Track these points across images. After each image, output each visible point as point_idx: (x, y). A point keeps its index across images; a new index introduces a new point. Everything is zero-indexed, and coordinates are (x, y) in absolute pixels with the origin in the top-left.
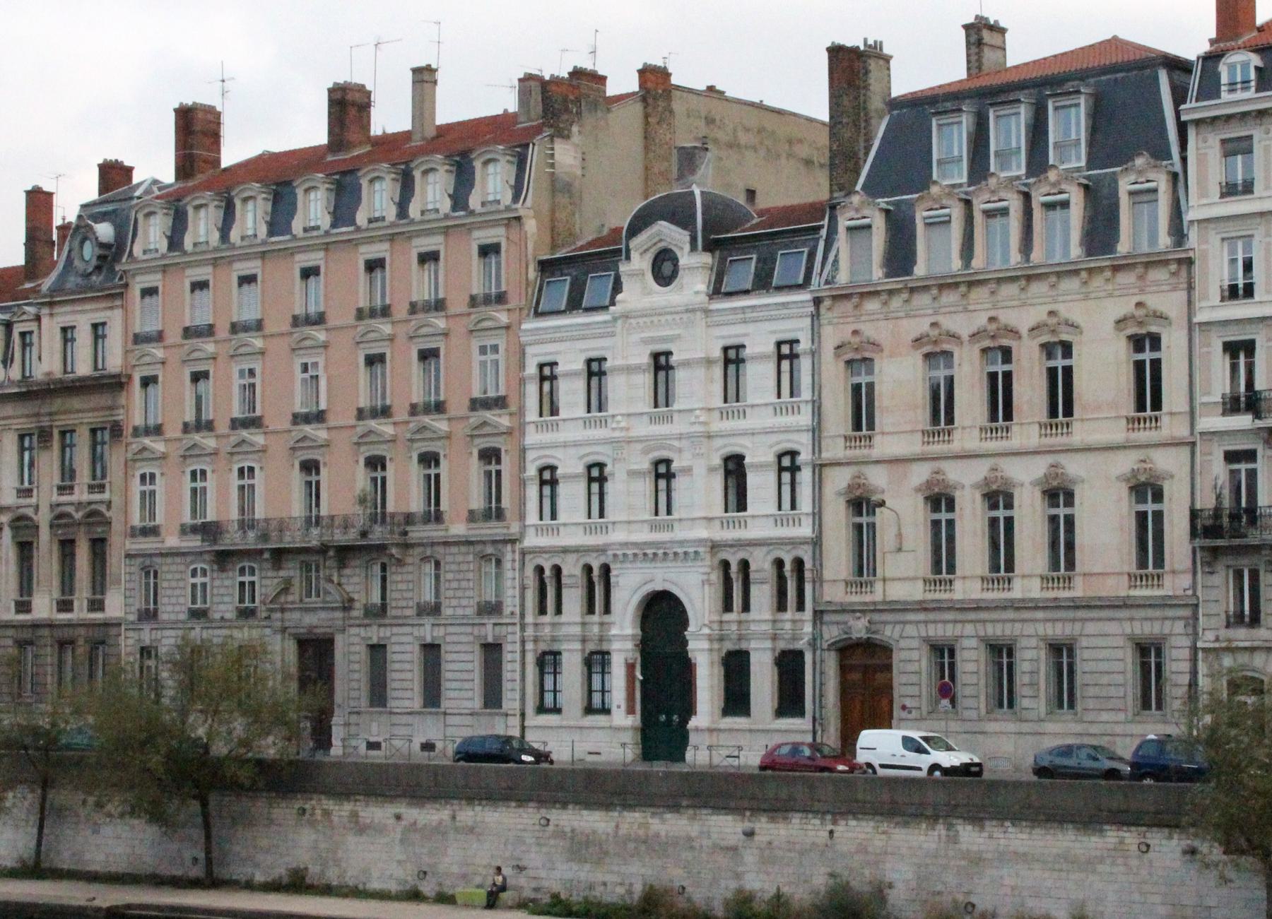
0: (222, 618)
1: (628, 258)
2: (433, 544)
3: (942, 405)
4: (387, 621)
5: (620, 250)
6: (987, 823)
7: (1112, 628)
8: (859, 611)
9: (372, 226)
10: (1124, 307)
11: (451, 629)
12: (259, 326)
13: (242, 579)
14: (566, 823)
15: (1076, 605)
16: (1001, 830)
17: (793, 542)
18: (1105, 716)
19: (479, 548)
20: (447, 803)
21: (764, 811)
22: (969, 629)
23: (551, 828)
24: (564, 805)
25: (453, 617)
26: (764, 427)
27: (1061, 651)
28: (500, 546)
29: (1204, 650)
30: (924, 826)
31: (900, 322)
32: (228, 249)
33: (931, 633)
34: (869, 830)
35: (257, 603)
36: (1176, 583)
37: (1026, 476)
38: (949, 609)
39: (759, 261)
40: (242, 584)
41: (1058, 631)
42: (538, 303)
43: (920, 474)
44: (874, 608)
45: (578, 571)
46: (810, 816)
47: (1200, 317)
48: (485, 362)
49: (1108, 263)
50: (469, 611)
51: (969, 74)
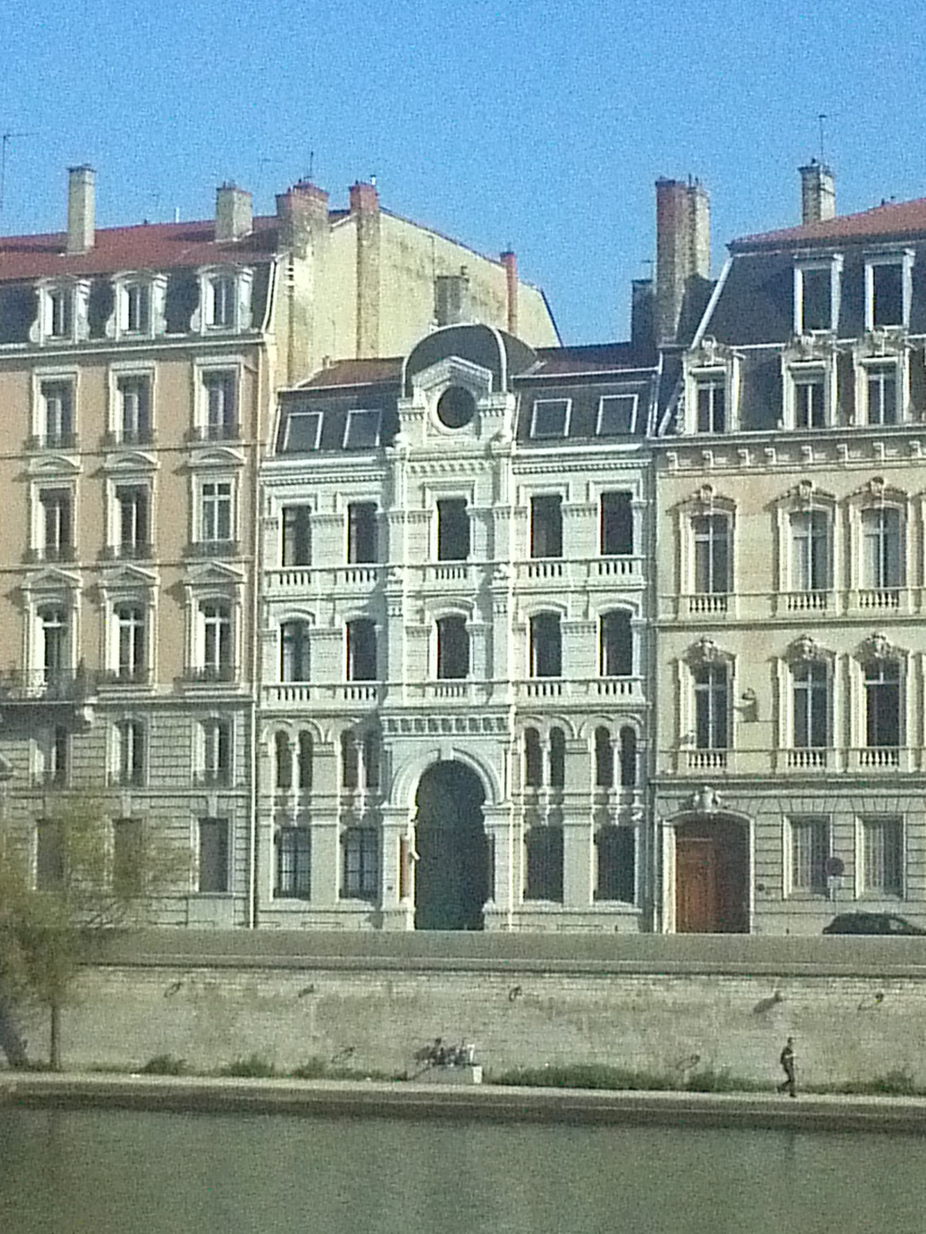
1: (410, 394)
17: (621, 710)
22: (844, 805)
26: (585, 584)
33: (870, 808)
42: (280, 441)
48: (211, 504)
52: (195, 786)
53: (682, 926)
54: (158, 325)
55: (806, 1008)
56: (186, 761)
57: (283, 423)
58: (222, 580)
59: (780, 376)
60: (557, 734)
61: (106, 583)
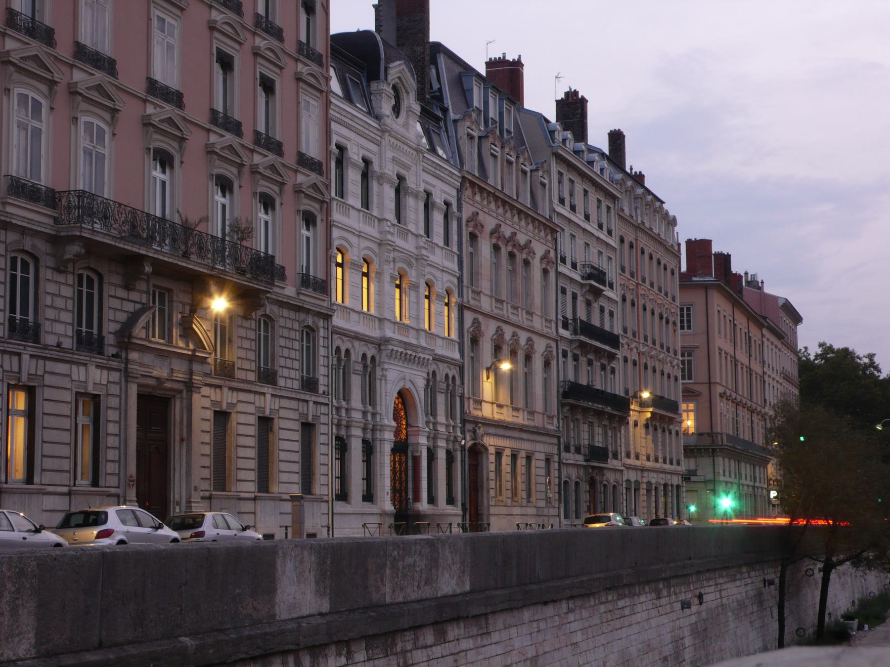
58: (109, 104)
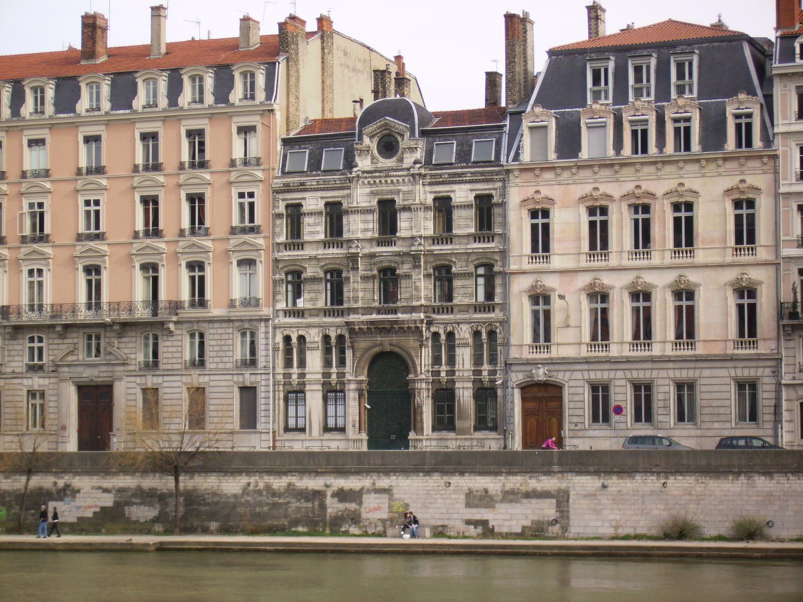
0: (13, 372)
2: (198, 322)
3: (599, 236)
4: (158, 373)
5: (354, 134)
6: (776, 475)
7: (723, 372)
8: (540, 364)
9: (145, 110)
10: (732, 181)
11: (213, 377)
12: (46, 173)
13: (32, 345)
14: (465, 485)
15: (698, 359)
16: (785, 478)
18: (716, 425)
19: (237, 324)
20: (367, 475)
21: (616, 472)
22: (620, 374)
23: (452, 488)
24: (462, 473)
25: (216, 369)
27: (685, 389)
28: (255, 323)
29: (786, 385)
30: (731, 478)
31: (569, 186)
32: (18, 121)
34: (692, 481)
35: (45, 360)
36: (764, 347)
37: (660, 283)
38: (606, 362)
39: (457, 145)
40: (31, 349)
41: (684, 375)
42: (284, 165)
43: (584, 280)
44: (551, 362)
45: (318, 339)
46: (648, 475)
47: (783, 190)
49: (721, 156)
50: (229, 366)
51: (590, 37)
52: (140, 369)
53: (525, 445)
54: (209, 99)
55: (620, 491)
56: (231, 354)
57: (285, 157)
59: (580, 128)
60: (301, 339)
61: (181, 250)
